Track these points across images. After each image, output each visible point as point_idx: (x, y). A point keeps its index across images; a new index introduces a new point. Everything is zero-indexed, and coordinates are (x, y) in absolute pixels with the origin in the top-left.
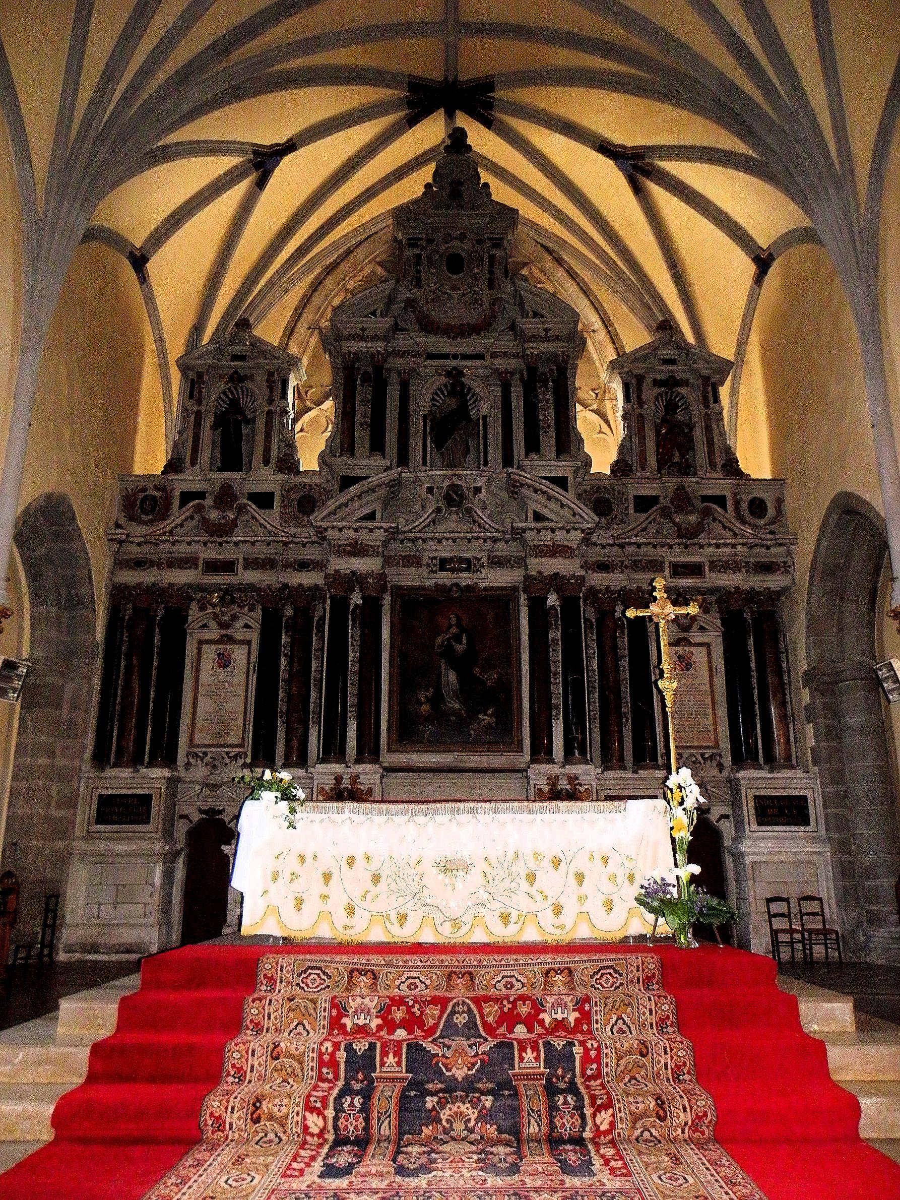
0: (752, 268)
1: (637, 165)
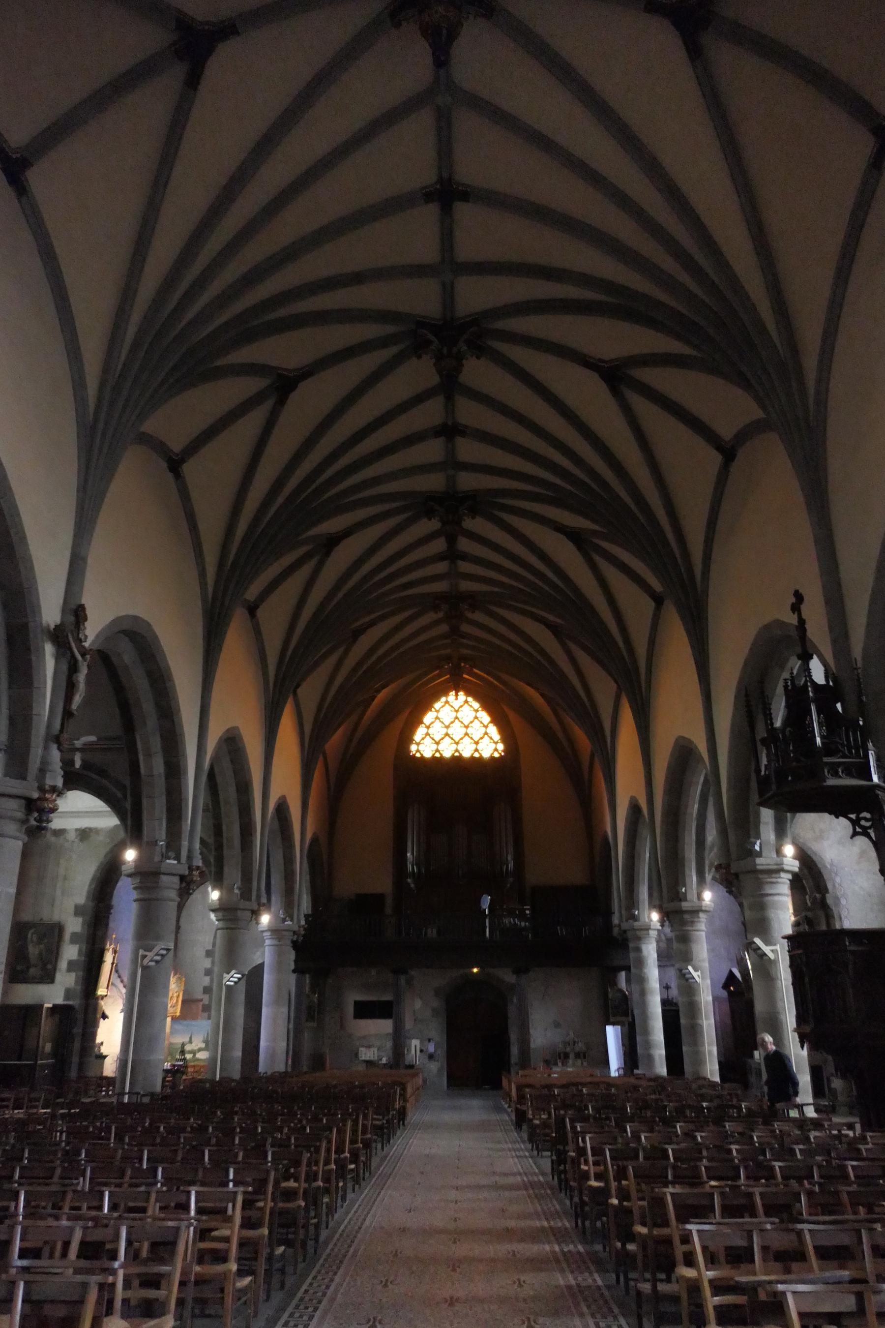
0: (717, 458)
1: (575, 537)
